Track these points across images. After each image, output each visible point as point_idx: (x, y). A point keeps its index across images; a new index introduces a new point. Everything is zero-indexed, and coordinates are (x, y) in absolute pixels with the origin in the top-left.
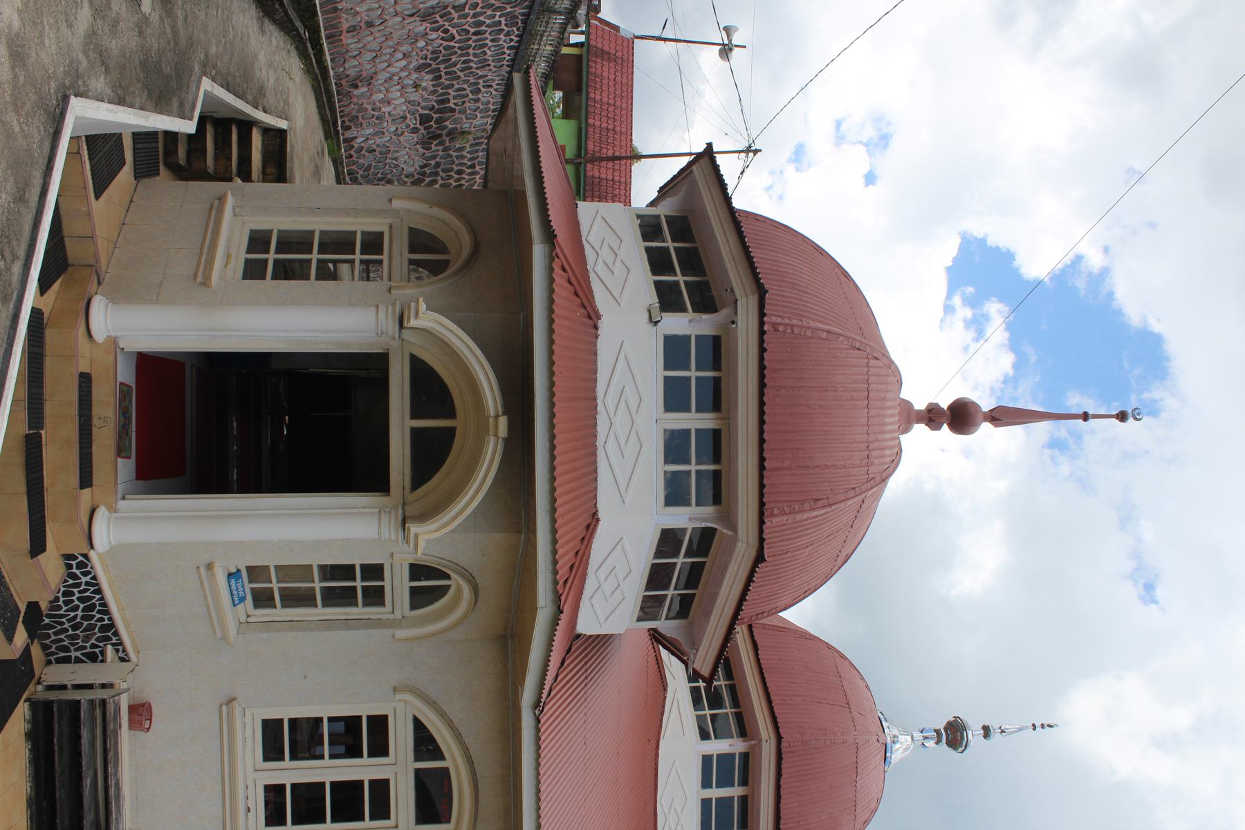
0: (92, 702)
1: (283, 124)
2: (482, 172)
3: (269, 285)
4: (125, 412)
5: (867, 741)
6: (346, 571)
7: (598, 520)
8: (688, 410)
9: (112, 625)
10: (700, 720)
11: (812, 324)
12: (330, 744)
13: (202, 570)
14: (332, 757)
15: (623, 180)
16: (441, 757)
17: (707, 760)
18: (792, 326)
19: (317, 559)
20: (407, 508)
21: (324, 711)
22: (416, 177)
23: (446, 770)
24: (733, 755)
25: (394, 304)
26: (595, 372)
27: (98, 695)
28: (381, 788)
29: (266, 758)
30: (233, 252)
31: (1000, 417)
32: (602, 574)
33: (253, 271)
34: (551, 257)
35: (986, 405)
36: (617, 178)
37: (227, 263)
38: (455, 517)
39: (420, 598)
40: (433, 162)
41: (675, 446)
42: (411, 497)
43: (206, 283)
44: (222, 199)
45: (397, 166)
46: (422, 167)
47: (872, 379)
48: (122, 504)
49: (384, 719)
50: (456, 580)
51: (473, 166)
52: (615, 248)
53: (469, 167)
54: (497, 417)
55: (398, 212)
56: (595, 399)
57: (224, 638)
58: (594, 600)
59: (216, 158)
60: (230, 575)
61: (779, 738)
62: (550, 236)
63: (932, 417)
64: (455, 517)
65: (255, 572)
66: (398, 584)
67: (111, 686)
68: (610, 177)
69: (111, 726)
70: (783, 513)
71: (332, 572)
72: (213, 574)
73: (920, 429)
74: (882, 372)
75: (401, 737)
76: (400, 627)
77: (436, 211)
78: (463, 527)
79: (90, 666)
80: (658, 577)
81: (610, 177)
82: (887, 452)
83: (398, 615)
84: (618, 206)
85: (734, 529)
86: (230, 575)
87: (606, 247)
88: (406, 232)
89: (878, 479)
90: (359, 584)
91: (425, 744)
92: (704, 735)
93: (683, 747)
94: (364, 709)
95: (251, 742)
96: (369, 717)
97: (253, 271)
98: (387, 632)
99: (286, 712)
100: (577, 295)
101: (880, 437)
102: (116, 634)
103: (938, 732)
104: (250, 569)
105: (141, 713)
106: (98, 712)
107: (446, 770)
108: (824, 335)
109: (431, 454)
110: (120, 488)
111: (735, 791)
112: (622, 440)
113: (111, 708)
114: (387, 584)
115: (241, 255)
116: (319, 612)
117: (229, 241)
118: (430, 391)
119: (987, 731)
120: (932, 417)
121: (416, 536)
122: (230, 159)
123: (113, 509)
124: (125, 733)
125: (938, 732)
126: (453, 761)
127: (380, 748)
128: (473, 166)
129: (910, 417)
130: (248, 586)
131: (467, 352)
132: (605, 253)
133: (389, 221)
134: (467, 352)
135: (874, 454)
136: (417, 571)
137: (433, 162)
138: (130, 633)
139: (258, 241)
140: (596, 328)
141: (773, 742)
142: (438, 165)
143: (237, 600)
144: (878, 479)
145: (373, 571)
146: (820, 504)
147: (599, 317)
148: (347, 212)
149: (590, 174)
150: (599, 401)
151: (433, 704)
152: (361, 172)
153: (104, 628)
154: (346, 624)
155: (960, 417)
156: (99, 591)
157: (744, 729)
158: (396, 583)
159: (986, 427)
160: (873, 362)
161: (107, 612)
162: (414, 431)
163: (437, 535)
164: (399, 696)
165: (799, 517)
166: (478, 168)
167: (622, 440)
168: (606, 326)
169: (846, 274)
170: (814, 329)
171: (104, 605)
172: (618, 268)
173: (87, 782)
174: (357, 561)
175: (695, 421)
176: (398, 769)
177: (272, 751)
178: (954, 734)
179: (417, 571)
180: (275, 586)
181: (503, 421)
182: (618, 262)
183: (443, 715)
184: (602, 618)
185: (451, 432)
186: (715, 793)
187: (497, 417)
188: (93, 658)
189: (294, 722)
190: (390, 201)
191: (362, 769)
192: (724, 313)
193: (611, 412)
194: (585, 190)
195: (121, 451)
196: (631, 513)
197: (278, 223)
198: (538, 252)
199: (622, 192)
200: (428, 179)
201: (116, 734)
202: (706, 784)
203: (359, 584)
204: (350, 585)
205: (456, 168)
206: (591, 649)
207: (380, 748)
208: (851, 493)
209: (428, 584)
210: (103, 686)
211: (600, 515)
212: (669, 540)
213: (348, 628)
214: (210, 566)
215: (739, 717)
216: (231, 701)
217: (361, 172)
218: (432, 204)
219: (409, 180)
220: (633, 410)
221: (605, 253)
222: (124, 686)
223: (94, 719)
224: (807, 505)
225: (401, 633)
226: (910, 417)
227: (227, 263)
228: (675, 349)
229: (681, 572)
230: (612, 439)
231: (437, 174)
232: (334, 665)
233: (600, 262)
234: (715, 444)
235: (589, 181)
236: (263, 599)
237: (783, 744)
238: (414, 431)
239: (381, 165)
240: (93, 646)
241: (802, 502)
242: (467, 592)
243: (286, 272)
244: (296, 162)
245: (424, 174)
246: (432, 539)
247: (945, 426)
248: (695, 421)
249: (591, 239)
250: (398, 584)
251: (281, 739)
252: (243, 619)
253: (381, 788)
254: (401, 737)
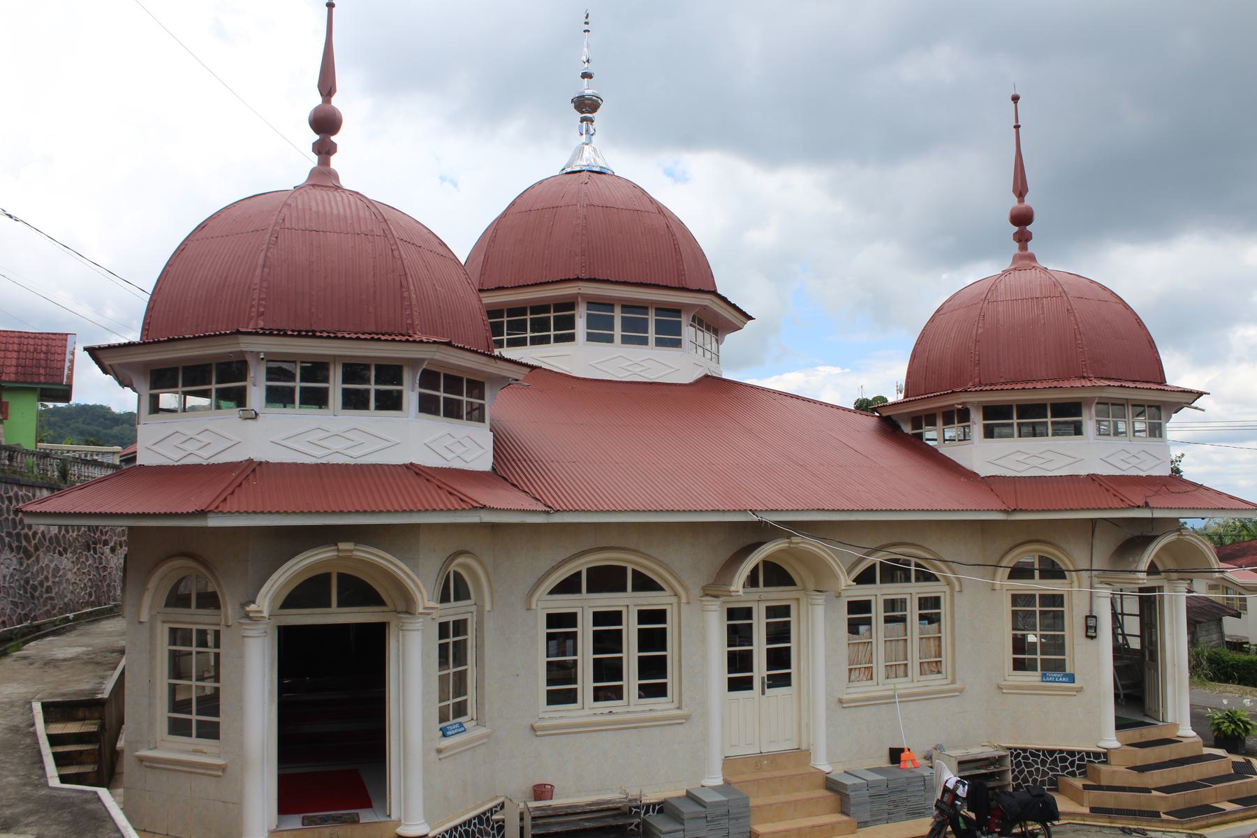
0: (533, 826)
1: (37, 707)
2: (16, 489)
3: (223, 719)
4: (324, 820)
5: (586, 195)
6: (443, 649)
7: (411, 464)
8: (326, 390)
9: (479, 817)
10: (558, 339)
11: (257, 280)
12: (564, 654)
13: (441, 756)
14: (575, 653)
15: (16, 340)
16: (579, 573)
17: (591, 338)
18: (260, 299)
19: (435, 672)
20: (399, 609)
21: (542, 660)
22: (21, 555)
23: (589, 570)
24: (588, 315)
25: (242, 624)
26: (296, 464)
27: (528, 822)
28: (599, 618)
29: (574, 701)
30: (191, 748)
31: (327, 86)
32: (450, 456)
33: (210, 731)
34: (218, 512)
35: (317, 100)
36: (16, 347)
37: (201, 752)
38: (401, 569)
39: (462, 592)
40: (7, 539)
41: (354, 401)
42: (390, 607)
43: (223, 768)
44: (141, 760)
45: (12, 576)
46: (12, 550)
47: (301, 226)
48: (394, 817)
49: (550, 616)
50: (452, 568)
51: (10, 499)
52: (185, 438)
53: (11, 502)
54: (338, 550)
55: (152, 616)
56: (317, 465)
57: (488, 736)
58: (468, 459)
59: (81, 763)
60: (444, 735)
61: (578, 279)
62: (202, 513)
63: (324, 150)
64: (401, 569)
65: (443, 718)
66: (453, 611)
67: (522, 814)
68: (15, 355)
69: (550, 812)
70: (411, 316)
71: (443, 661)
72: (446, 748)
73: (335, 162)
74: (295, 214)
75: (563, 604)
76: (483, 606)
77: (152, 585)
78: (414, 568)
79: (507, 830)
80: (453, 411)
81: (15, 355)
82: (361, 214)
83: (474, 608)
84: (141, 430)
85: (423, 360)
86: (444, 735)
87: (184, 446)
88: (170, 610)
89: (385, 226)
90: (451, 640)
91: (569, 586)
92: (571, 338)
93: (578, 357)
94: (542, 630)
95: (565, 713)
96: (548, 627)
97: (210, 731)
98: (486, 616)
99: (543, 688)
100: (240, 485)
101: (349, 221)
102: (484, 813)
103: (583, 120)
104: (441, 721)
105: (541, 792)
106: (540, 822)
107: (589, 570)
108: (266, 270)
109: (358, 591)
110: (382, 819)
111: (618, 315)
112: (350, 444)
113: (537, 813)
114: (451, 619)
115: (194, 742)
116: (470, 667)
117: (187, 752)
118: (309, 592)
119: (586, 75)
120: (324, 150)
121: (425, 608)
122: (81, 752)
123: (398, 823)
124: (555, 802)
125: (583, 120)
126: (582, 565)
127: (571, 619)
128: (10, 499)
129: (323, 177)
130: (452, 721)
131: (288, 574)
132: (190, 447)
133: (159, 624)
134: (288, 574)
135: (363, 229)
136: (444, 598)
137: (7, 539)
138: (483, 804)
139: (179, 728)
140: (260, 463)
141: (580, 284)
142: (9, 534)
143: (462, 729)
144: (385, 226)
145: (443, 629)
146: (404, 283)
147: (250, 461)
148: (152, 656)
149: (13, 377)
150: (319, 461)
151: (540, 581)
152: (19, 611)
153: (481, 823)
154: (479, 647)
155: (325, 124)
156: (456, 828)
157: (569, 305)
158: (451, 611)
159: (336, 101)
160: (287, 224)
161: (470, 821)
162: (340, 605)
163: (425, 593)
164: (534, 606)
165: (414, 302)
166: (11, 494)
167: (350, 444)
168: (259, 455)
169: (201, 227)
170: (262, 280)
171: (465, 823)
172: (205, 438)
173: (588, 825)
174: (436, 642)
175: (336, 386)
176: (585, 605)
177: (570, 697)
178: (586, 106)
179: (444, 598)
180: (451, 702)
181: (342, 546)
182: (199, 437)
183: (548, 574)
184: (482, 451)
185: (340, 576)
186: (618, 332)
187: (338, 550)
188: (501, 828)
189: (550, 682)
190: (141, 623)
191: (585, 631)
192: (249, 358)
193: (326, 452)
194: (32, 382)
195: (355, 821)
196: (410, 437)
197: (162, 713)
198: (213, 522)
199: (31, 341)
200: (24, 543)
201: (556, 808)
202: (610, 339)
203: (451, 640)
204: (453, 646)
205: (12, 516)
206: (509, 464)
207: (571, 619)
208: (396, 253)
209: (453, 589)
210: (522, 819)
211: (407, 462)
212: (428, 406)
213: (483, 645)
214: (439, 751)
215: (558, 307)
216: (533, 729)
217: (19, 611)
218: (144, 588)
219: (25, 562)
220: (327, 434)
221: (190, 447)
222: (522, 805)
223: (544, 824)
224: (406, 294)
225: (488, 607)
226: (323, 177)
227: (201, 752)
228: (278, 397)
229: (452, 395)
230: (347, 452)
231: (18, 535)
232: (513, 656)
233: (199, 453)
234: (354, 371)
235: (21, 378)
236: (460, 710)
237: (583, 276)
238: (340, 605)
239: (11, 591)
240: (493, 829)
241: (402, 298)
242: (460, 560)
243: (210, 704)
244: (64, 690)
245: (19, 548)
246: (425, 596)
247: (333, 138)
248: (336, 386)
249: (176, 457)
250: (453, 611)
251: (561, 695)
252: (474, 723)
253: (644, 616)
254: (563, 604)
